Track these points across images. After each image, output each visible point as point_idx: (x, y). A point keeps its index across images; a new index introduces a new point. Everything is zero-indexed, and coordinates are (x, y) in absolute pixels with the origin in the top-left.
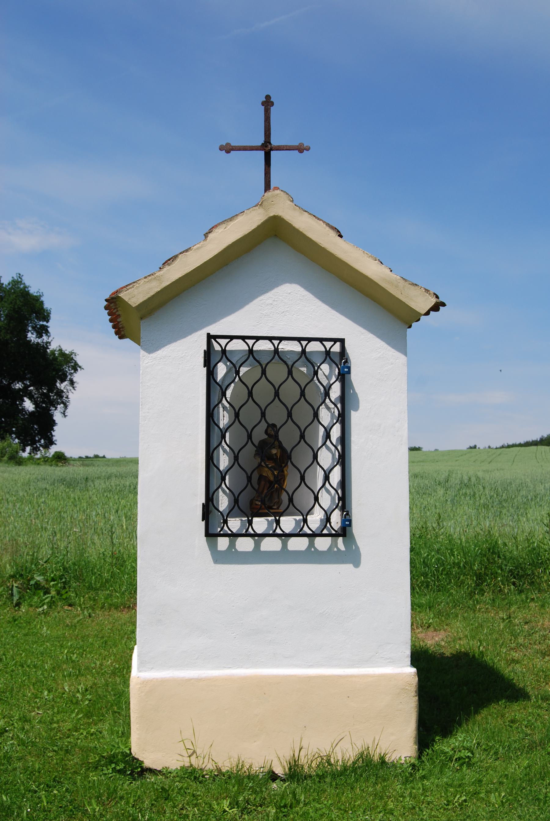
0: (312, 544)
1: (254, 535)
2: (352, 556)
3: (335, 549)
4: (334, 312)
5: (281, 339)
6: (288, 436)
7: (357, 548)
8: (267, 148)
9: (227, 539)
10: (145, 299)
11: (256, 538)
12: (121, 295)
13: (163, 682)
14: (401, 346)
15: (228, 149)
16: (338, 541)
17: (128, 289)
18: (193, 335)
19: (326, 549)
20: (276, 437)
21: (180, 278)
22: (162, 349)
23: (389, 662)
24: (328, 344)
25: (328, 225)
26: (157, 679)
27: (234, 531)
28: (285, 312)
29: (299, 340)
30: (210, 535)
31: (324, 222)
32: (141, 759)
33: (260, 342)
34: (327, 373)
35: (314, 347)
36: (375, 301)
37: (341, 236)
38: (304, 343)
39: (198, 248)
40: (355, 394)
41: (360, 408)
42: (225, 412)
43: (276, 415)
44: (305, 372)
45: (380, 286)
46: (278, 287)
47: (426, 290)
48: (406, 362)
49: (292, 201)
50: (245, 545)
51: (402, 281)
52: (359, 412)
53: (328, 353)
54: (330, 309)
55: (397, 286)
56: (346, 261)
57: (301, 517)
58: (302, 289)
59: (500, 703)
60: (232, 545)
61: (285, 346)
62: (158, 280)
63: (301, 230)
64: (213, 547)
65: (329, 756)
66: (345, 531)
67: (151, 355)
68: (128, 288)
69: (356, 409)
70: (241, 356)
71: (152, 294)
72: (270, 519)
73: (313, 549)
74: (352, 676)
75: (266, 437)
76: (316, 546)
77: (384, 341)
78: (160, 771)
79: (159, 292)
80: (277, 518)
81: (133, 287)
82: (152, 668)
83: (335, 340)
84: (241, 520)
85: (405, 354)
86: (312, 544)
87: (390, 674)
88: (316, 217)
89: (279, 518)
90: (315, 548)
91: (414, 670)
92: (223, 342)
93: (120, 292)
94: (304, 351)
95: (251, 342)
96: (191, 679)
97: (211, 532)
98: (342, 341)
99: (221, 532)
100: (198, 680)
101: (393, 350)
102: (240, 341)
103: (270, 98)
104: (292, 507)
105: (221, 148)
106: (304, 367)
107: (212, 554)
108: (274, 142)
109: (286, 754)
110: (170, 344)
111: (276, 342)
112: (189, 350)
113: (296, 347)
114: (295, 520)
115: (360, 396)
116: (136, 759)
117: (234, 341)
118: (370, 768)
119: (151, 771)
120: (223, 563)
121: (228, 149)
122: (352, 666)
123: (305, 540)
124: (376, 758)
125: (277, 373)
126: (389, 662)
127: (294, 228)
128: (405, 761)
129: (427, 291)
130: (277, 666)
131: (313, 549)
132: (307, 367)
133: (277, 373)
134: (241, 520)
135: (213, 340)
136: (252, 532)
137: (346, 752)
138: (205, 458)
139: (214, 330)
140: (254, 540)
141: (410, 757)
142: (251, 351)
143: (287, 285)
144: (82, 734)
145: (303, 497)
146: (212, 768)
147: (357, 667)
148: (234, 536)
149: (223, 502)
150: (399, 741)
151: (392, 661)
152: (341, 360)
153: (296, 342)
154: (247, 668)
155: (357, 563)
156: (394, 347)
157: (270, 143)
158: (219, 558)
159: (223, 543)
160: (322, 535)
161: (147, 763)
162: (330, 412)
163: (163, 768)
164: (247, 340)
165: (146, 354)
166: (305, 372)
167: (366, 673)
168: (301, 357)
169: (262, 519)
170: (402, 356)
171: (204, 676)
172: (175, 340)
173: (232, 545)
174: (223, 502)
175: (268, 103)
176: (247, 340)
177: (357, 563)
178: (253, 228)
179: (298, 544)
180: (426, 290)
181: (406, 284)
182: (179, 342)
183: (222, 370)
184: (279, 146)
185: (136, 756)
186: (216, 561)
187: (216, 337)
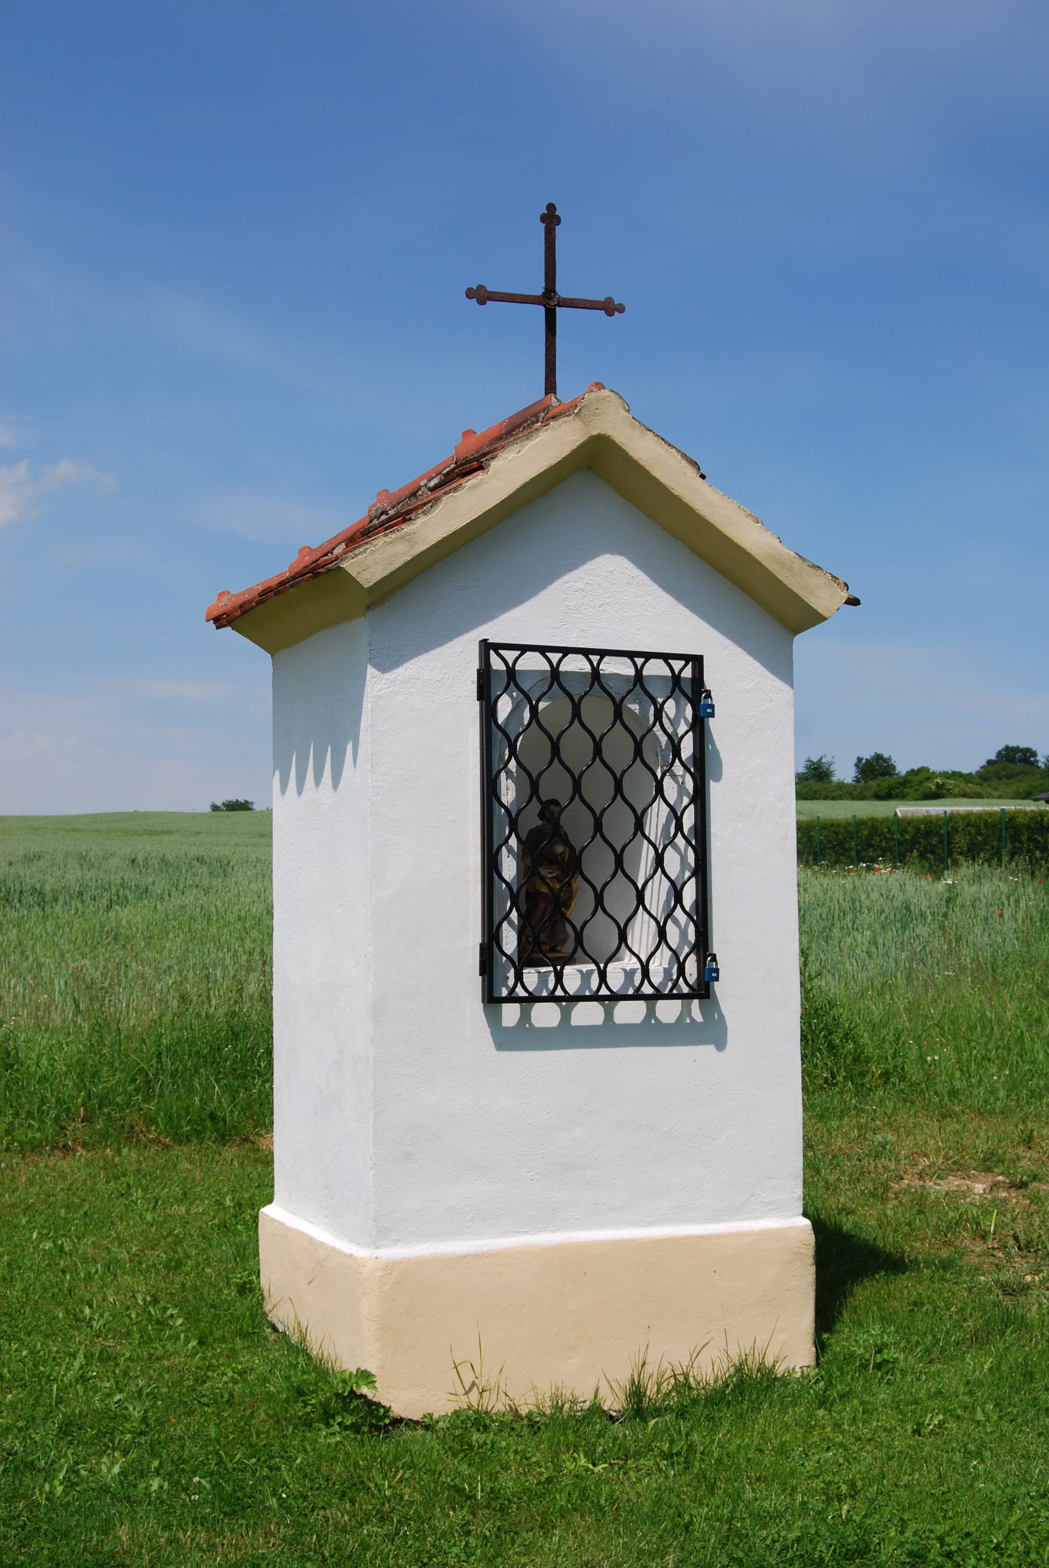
0: (651, 1012)
1: (681, 996)
2: (713, 1032)
3: (688, 1021)
4: (681, 608)
5: (603, 653)
6: (576, 823)
7: (722, 1017)
8: (550, 301)
9: (517, 1006)
10: (385, 574)
11: (564, 1004)
12: (345, 565)
13: (419, 1264)
14: (782, 667)
15: (481, 295)
16: (693, 1007)
17: (356, 555)
18: (456, 640)
19: (673, 1021)
20: (557, 826)
21: (444, 538)
22: (405, 665)
23: (772, 1210)
24: (677, 665)
25: (684, 456)
26: (409, 1259)
27: (572, 991)
28: (605, 606)
29: (631, 655)
30: (491, 999)
31: (679, 451)
32: (384, 1403)
33: (571, 657)
34: (672, 716)
35: (655, 668)
36: (744, 591)
37: (703, 477)
38: (639, 661)
39: (474, 486)
40: (716, 751)
41: (724, 776)
42: (509, 781)
43: (556, 786)
44: (637, 711)
45: (764, 567)
46: (592, 559)
47: (833, 577)
48: (792, 699)
49: (628, 411)
50: (546, 1015)
51: (798, 561)
52: (721, 782)
53: (676, 678)
54: (675, 602)
55: (790, 570)
56: (716, 525)
57: (593, 967)
58: (632, 565)
59: (877, 1276)
60: (525, 1016)
61: (610, 666)
62: (409, 541)
63: (642, 463)
64: (494, 1019)
65: (686, 1376)
66: (703, 990)
67: (387, 676)
68: (356, 552)
69: (718, 778)
70: (535, 681)
71: (397, 565)
72: (543, 970)
73: (653, 1021)
74: (719, 1236)
75: (540, 823)
76: (658, 1015)
77: (759, 661)
78: (417, 1422)
79: (409, 562)
80: (559, 968)
81: (365, 551)
82: (398, 1241)
83: (687, 658)
84: (580, 971)
85: (792, 686)
86: (651, 1012)
87: (777, 1230)
88: (666, 442)
89: (562, 969)
90: (657, 1019)
91: (807, 1222)
92: (510, 655)
93: (342, 560)
94: (595, 670)
95: (555, 657)
96: (466, 1256)
97: (496, 995)
98: (697, 661)
99: (675, 992)
100: (478, 1256)
101: (772, 677)
102: (537, 655)
103: (555, 209)
104: (579, 951)
105: (470, 294)
106: (636, 703)
107: (492, 1034)
108: (563, 290)
109: (623, 1377)
110: (417, 656)
111: (595, 658)
112: (454, 665)
113: (624, 668)
114: (580, 971)
115: (723, 755)
116: (375, 1403)
117: (528, 654)
118: (750, 1388)
119: (398, 1421)
120: (510, 1050)
121: (481, 295)
122: (716, 1219)
123: (641, 1005)
124: (613, 1402)
125: (597, 713)
126: (772, 1210)
127: (631, 458)
128: (802, 1373)
129: (835, 578)
130: (602, 1226)
131: (653, 1021)
132: (640, 704)
133: (597, 713)
134: (539, 973)
135: (492, 652)
136: (563, 994)
137: (710, 1369)
138: (479, 863)
139: (496, 631)
140: (561, 1007)
141: (808, 1367)
142: (555, 673)
143: (608, 556)
144: (224, 1374)
145: (600, 933)
146: (502, 1409)
147: (724, 1221)
148: (532, 999)
149: (510, 941)
150: (789, 1343)
151: (775, 1209)
152: (694, 690)
153: (626, 660)
154: (553, 1232)
155: (721, 1044)
156: (773, 672)
157: (554, 292)
158: (506, 1040)
159: (511, 1013)
160: (670, 996)
161: (399, 1409)
162: (677, 782)
163: (425, 1416)
164: (501, 652)
165: (377, 673)
166: (637, 711)
167: (740, 1229)
168: (635, 686)
169: (533, 970)
170: (787, 688)
171: (485, 1249)
172: (426, 650)
173: (525, 1016)
174: (510, 941)
175: (551, 219)
176: (501, 652)
177: (721, 1044)
178: (564, 455)
179: (588, 1014)
180: (833, 577)
181: (804, 565)
182: (432, 652)
183: (504, 707)
184: (571, 299)
185: (375, 1400)
186: (500, 1046)
187: (497, 647)
